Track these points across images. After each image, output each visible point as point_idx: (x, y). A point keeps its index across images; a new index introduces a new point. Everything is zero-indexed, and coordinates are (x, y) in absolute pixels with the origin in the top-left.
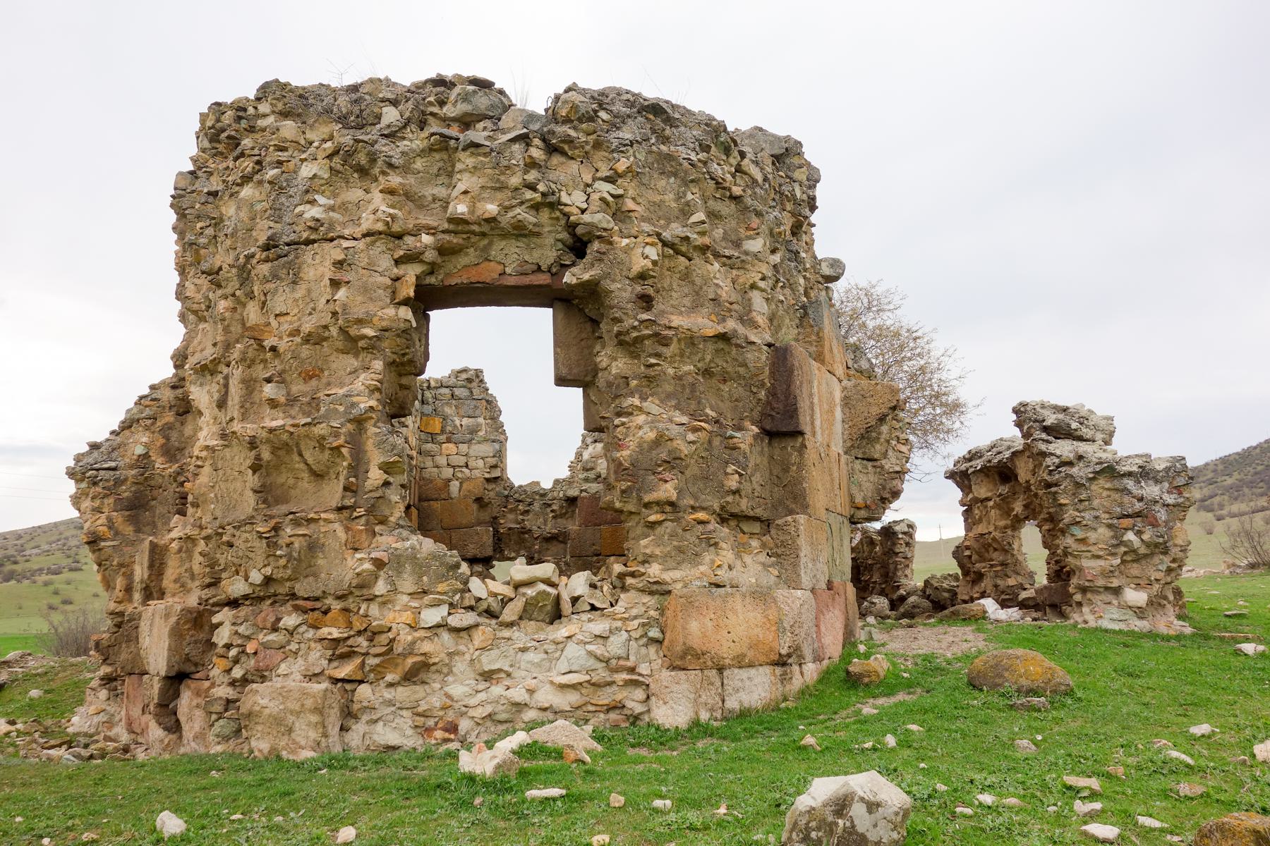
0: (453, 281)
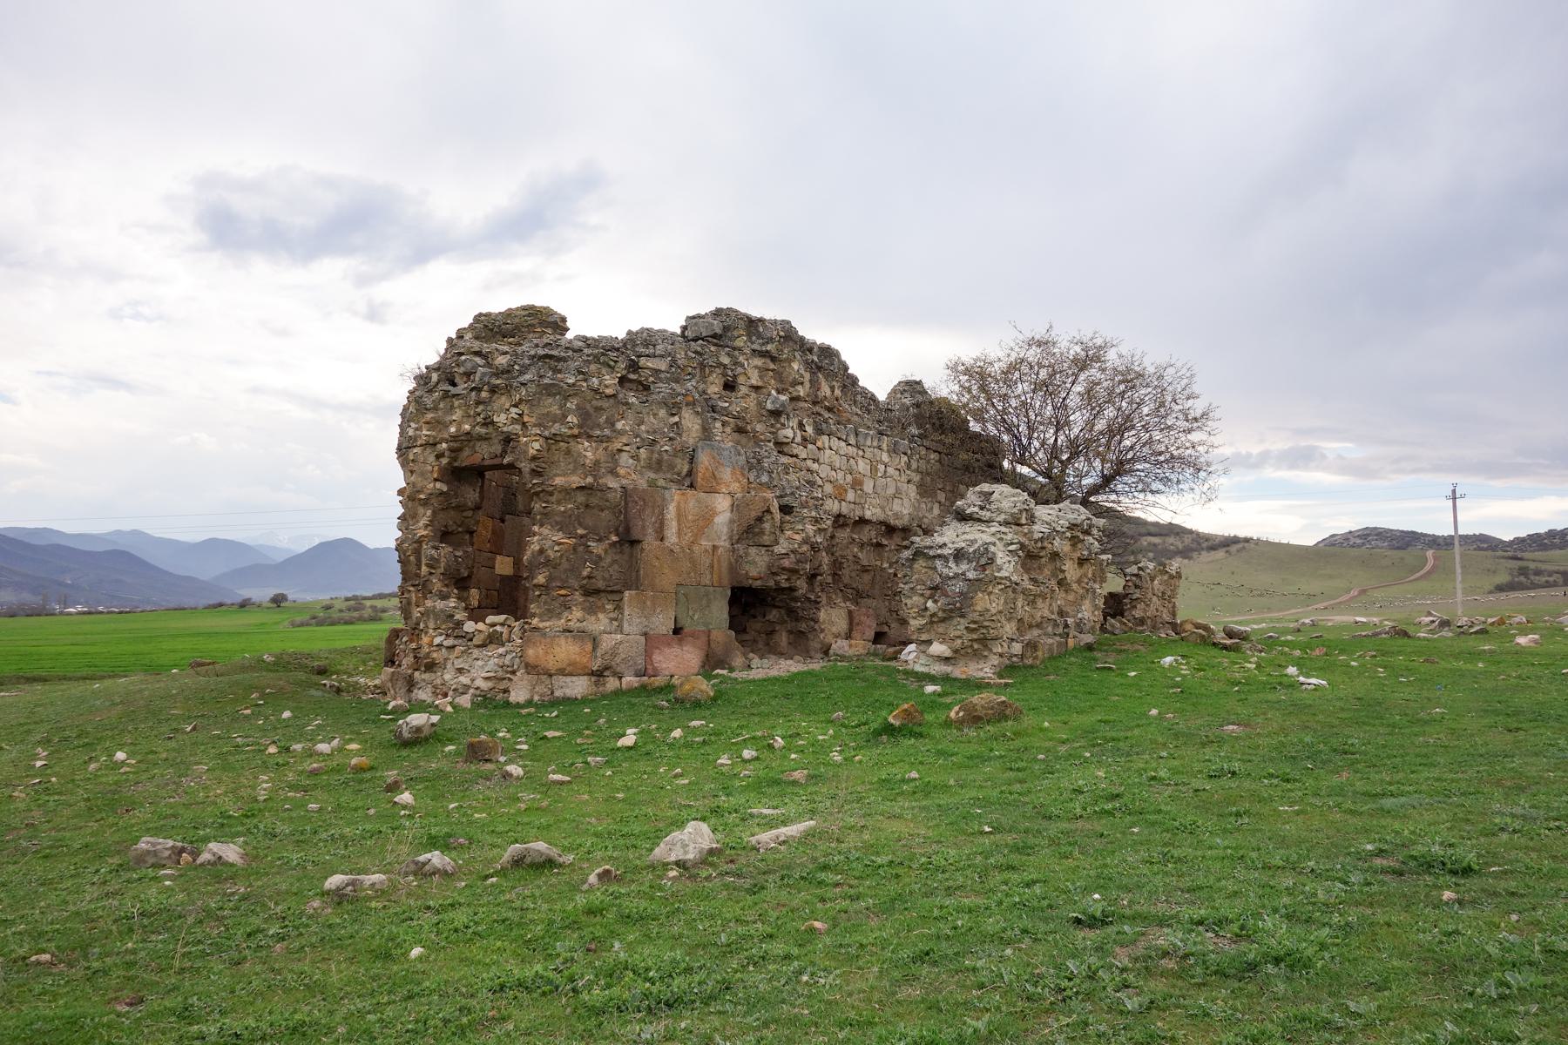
0: (464, 465)
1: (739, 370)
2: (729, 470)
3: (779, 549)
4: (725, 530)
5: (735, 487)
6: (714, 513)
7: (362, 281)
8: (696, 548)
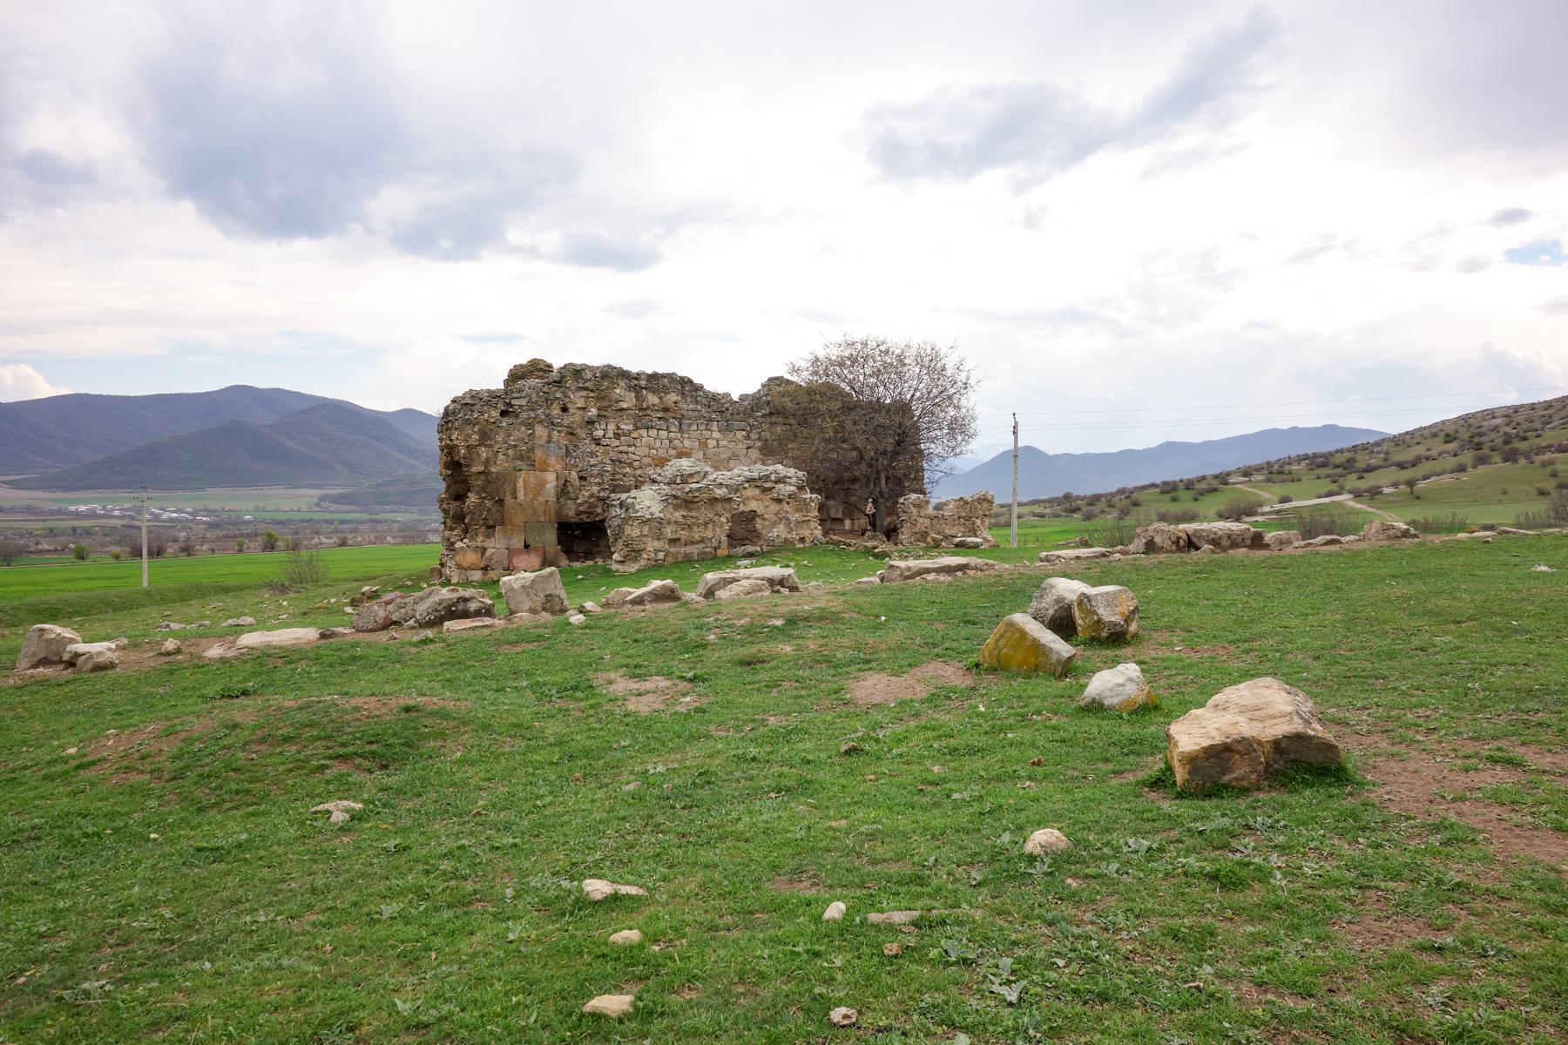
3: (579, 501)
5: (558, 467)
6: (546, 482)
7: (1021, 187)
8: (535, 502)
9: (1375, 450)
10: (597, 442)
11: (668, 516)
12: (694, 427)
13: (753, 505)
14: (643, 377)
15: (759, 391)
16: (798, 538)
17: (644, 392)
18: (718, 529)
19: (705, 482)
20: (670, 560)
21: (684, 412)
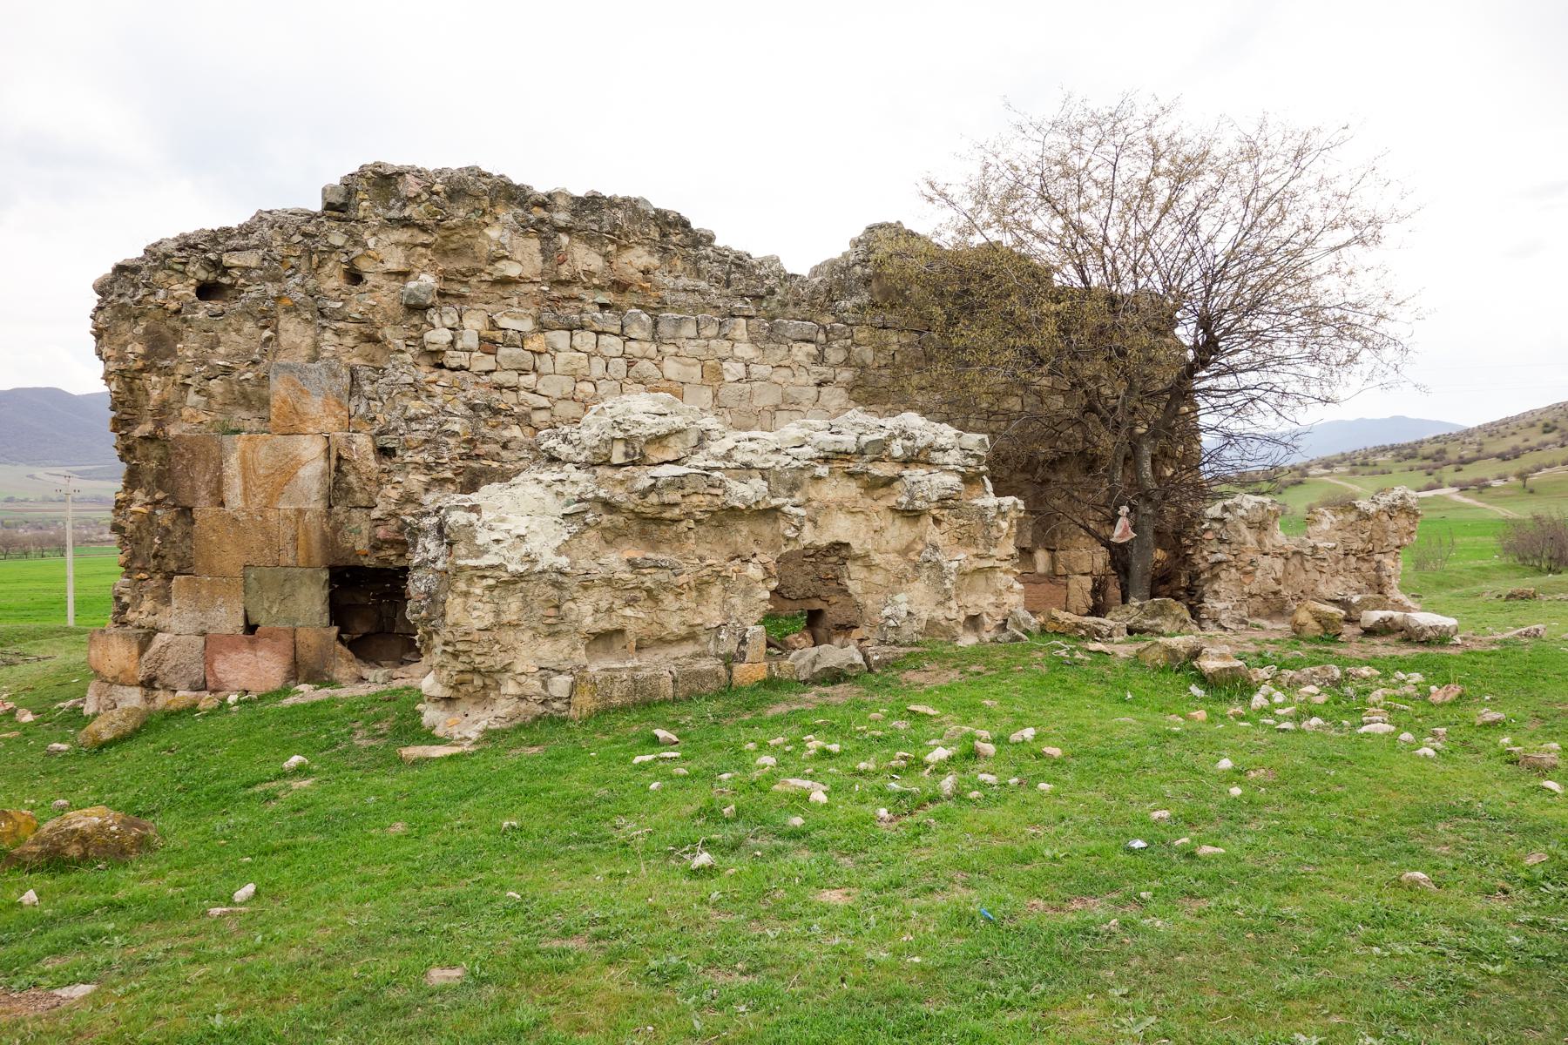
1: (358, 251)
2: (319, 400)
3: (376, 514)
4: (316, 486)
5: (329, 424)
8: (271, 514)
9: (1467, 440)
10: (436, 359)
11: (584, 563)
12: (689, 330)
13: (840, 528)
14: (560, 201)
15: (845, 255)
16: (962, 618)
17: (564, 239)
18: (736, 600)
19: (699, 460)
20: (586, 702)
21: (666, 294)
